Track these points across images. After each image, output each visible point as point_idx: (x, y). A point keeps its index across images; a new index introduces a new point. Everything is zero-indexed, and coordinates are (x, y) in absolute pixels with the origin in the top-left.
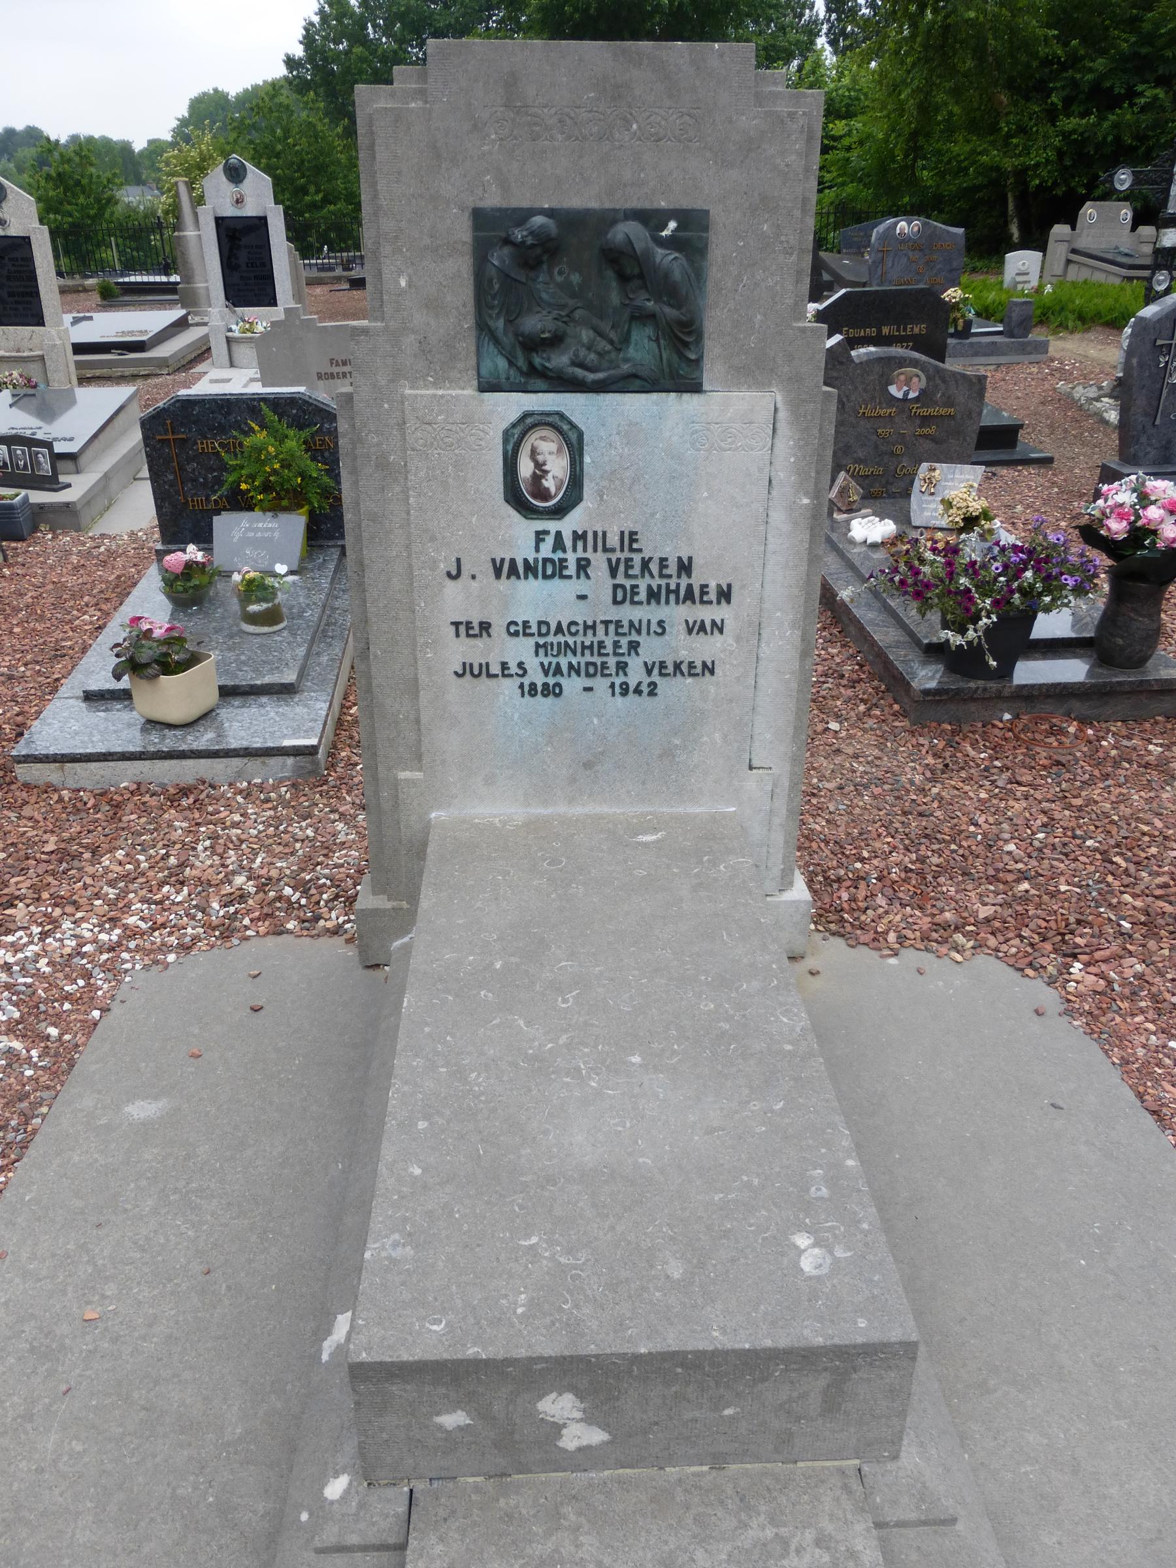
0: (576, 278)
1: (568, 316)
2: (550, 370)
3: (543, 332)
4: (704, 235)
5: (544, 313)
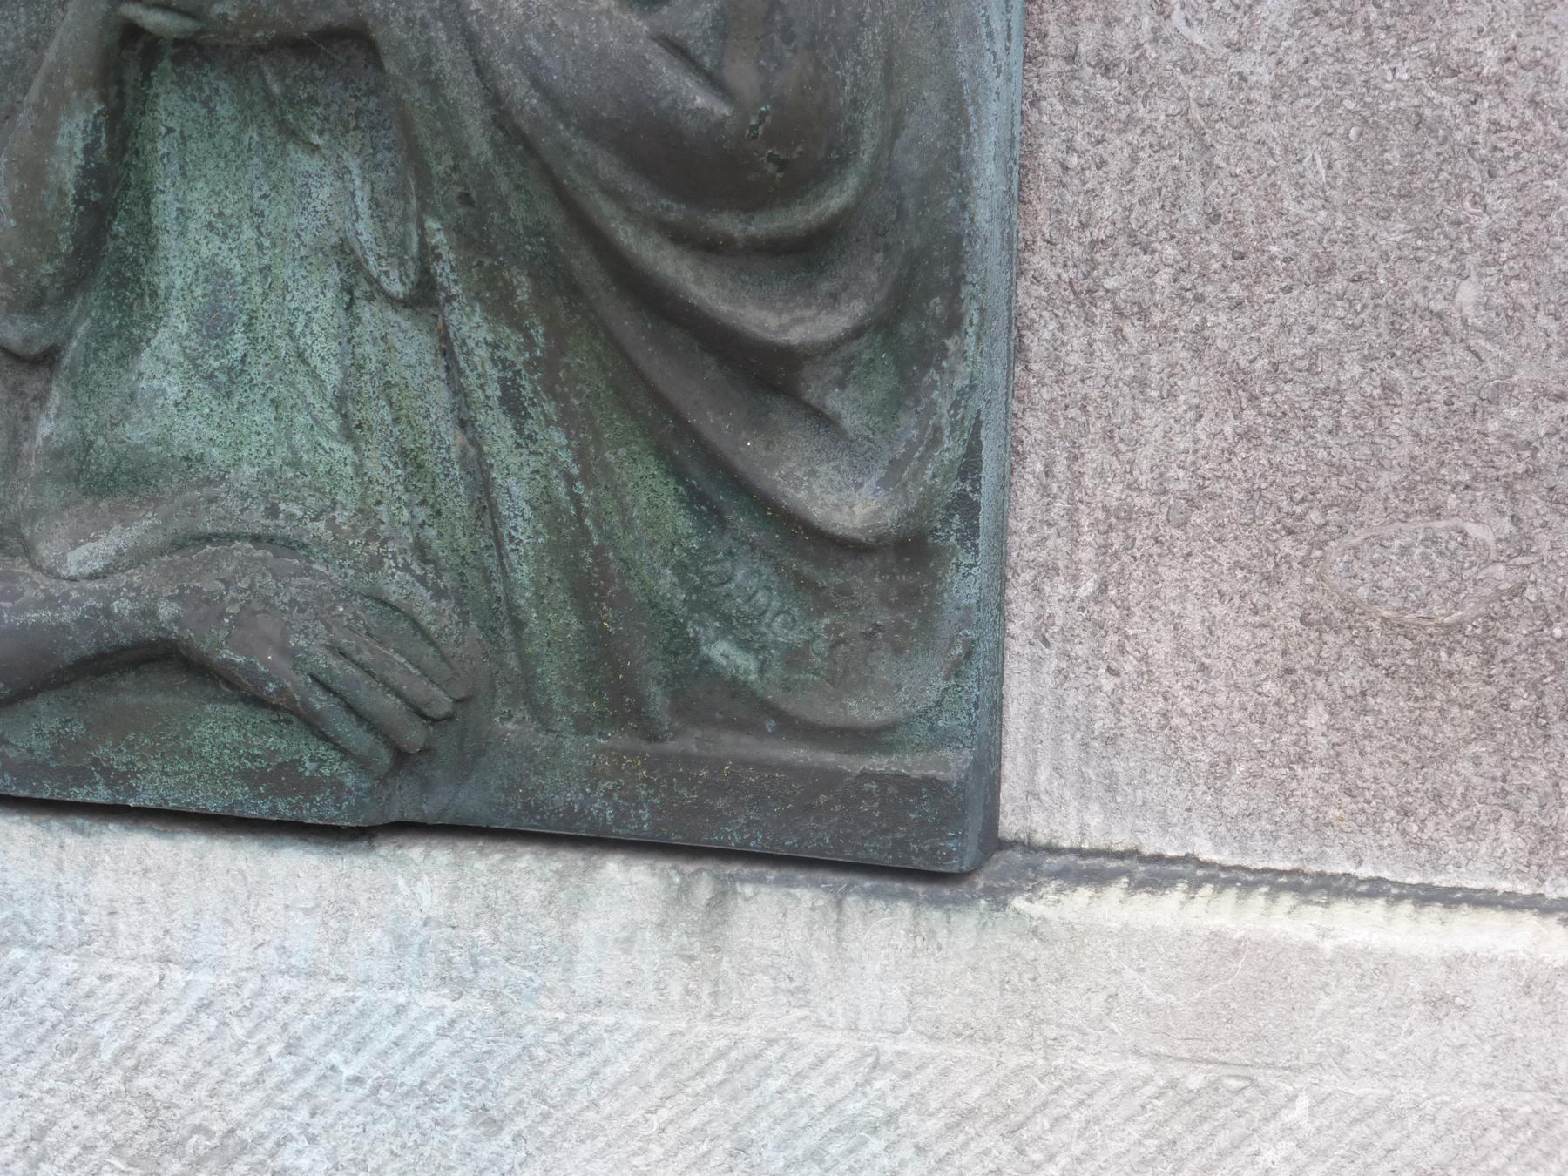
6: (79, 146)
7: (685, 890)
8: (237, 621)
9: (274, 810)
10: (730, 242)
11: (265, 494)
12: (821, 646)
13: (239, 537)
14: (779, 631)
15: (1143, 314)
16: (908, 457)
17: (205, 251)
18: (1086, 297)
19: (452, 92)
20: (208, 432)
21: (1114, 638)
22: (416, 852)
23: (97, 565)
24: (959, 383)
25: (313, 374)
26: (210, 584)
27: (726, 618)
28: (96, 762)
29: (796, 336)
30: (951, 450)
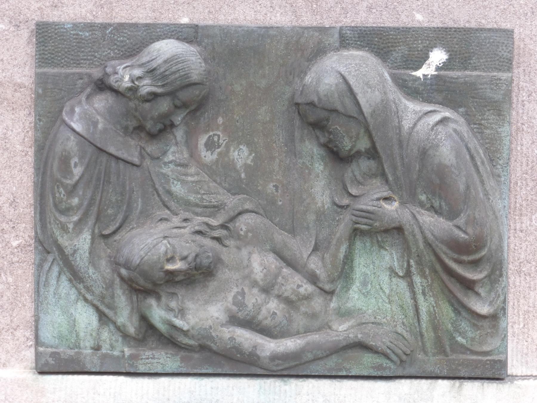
0: (241, 156)
1: (223, 226)
2: (185, 333)
3: (170, 260)
4: (504, 76)
5: (176, 221)
6: (344, 251)
7: (454, 384)
8: (373, 337)
9: (378, 374)
10: (465, 261)
11: (373, 315)
12: (478, 337)
13: (370, 323)
14: (470, 334)
15: (530, 275)
16: (493, 300)
17: (363, 271)
18: (519, 272)
19: (417, 237)
20: (363, 304)
21: (526, 335)
22: (403, 381)
23: (345, 329)
24: (503, 286)
25: (384, 292)
26: (367, 331)
27: (460, 333)
28: (344, 367)
29: (475, 278)
30: (502, 298)
